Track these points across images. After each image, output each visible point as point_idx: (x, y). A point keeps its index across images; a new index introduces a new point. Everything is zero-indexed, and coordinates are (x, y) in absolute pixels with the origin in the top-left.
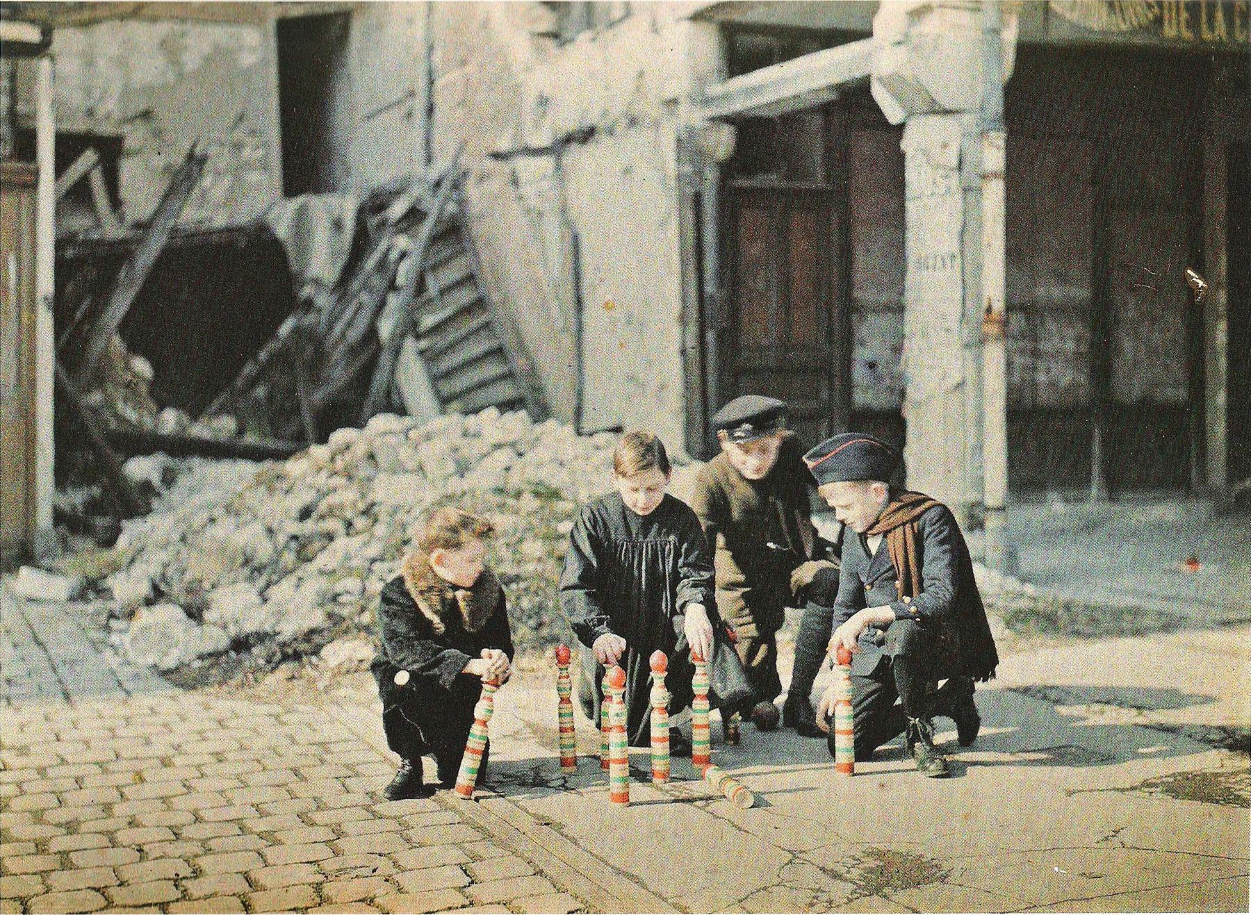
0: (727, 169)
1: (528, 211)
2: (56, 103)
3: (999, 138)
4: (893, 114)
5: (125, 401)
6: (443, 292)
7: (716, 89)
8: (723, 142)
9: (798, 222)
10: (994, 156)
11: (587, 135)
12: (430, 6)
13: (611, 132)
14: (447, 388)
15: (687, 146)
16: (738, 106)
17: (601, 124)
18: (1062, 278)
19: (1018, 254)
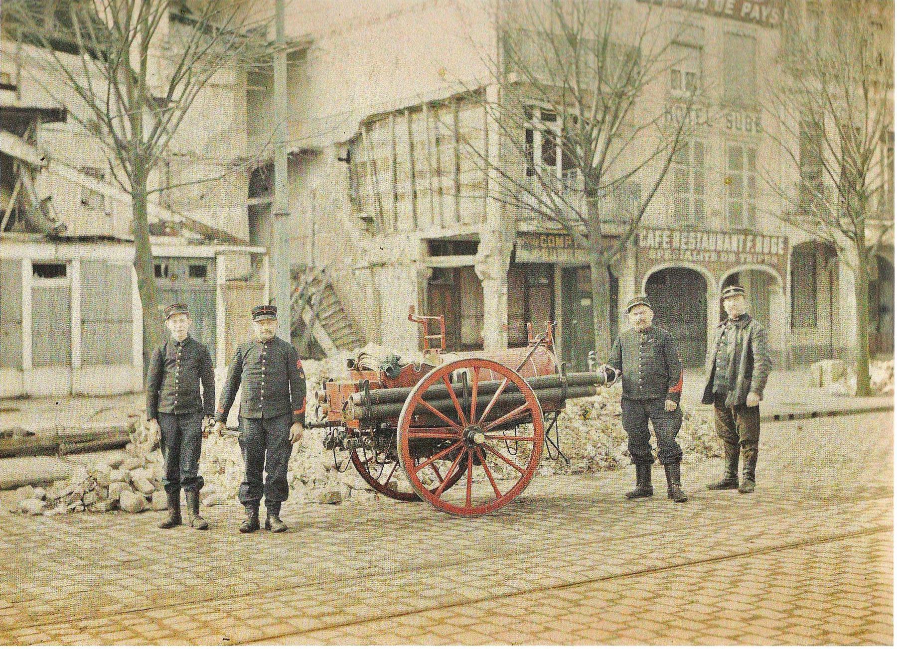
0: (429, 279)
1: (358, 283)
2: (8, 202)
3: (506, 285)
4: (481, 277)
5: (384, 516)
6: (329, 306)
7: (428, 259)
8: (430, 273)
9: (448, 293)
10: (505, 290)
11: (383, 265)
12: (890, 409)
13: (392, 265)
14: (333, 336)
15: (419, 274)
16: (435, 265)
17: (388, 262)
18: (719, 386)
19: (510, 306)
